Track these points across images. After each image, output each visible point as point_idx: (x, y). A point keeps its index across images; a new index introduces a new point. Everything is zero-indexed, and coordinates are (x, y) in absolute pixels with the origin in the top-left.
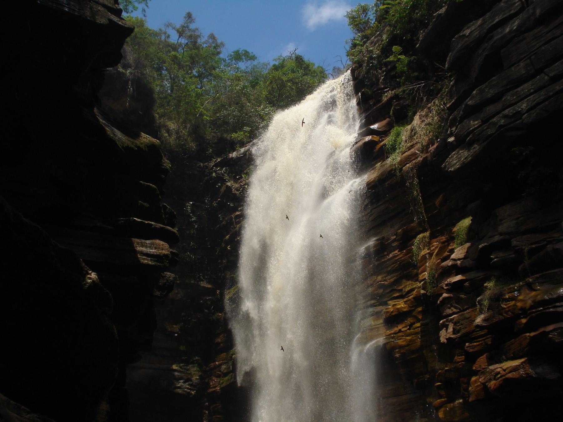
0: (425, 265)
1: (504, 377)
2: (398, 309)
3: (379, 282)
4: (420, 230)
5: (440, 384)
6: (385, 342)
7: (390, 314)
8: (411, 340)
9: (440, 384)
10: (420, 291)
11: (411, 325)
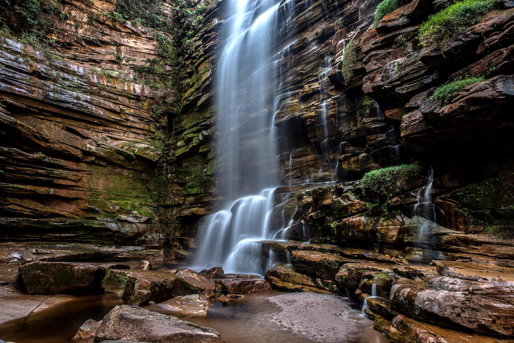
2: (313, 89)
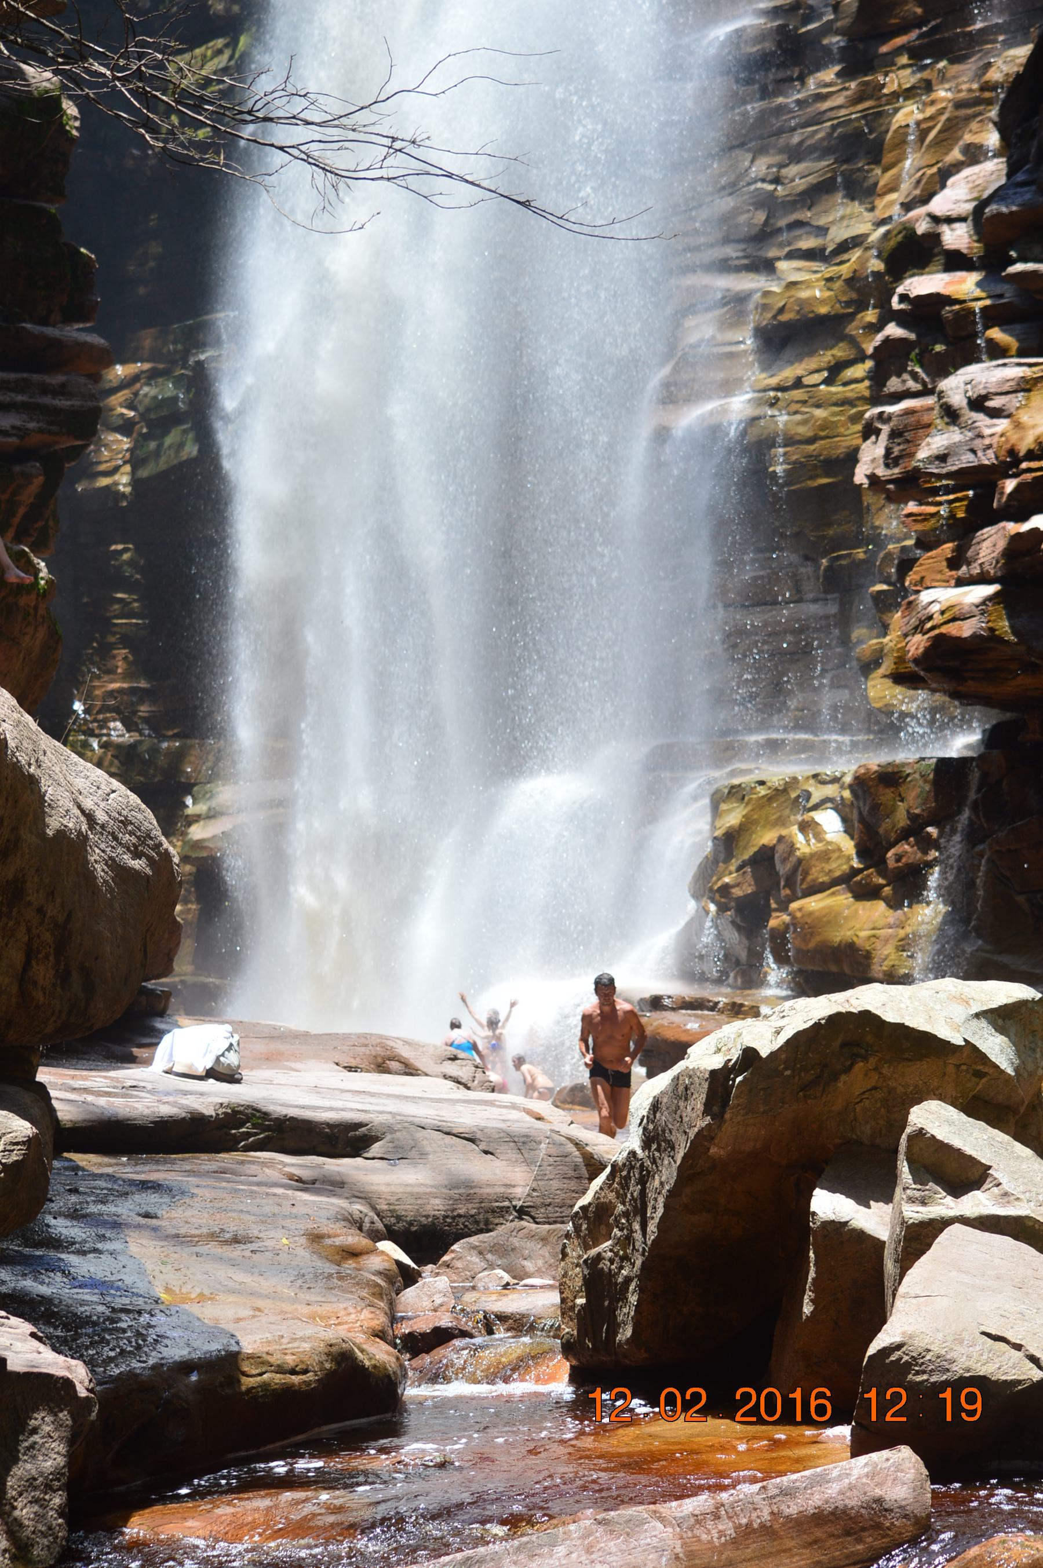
0: (900, 165)
1: (937, 632)
2: (802, 303)
3: (755, 181)
4: (915, 13)
5: (885, 587)
6: (750, 412)
7: (774, 317)
8: (826, 425)
9: (885, 587)
10: (867, 260)
11: (835, 371)
